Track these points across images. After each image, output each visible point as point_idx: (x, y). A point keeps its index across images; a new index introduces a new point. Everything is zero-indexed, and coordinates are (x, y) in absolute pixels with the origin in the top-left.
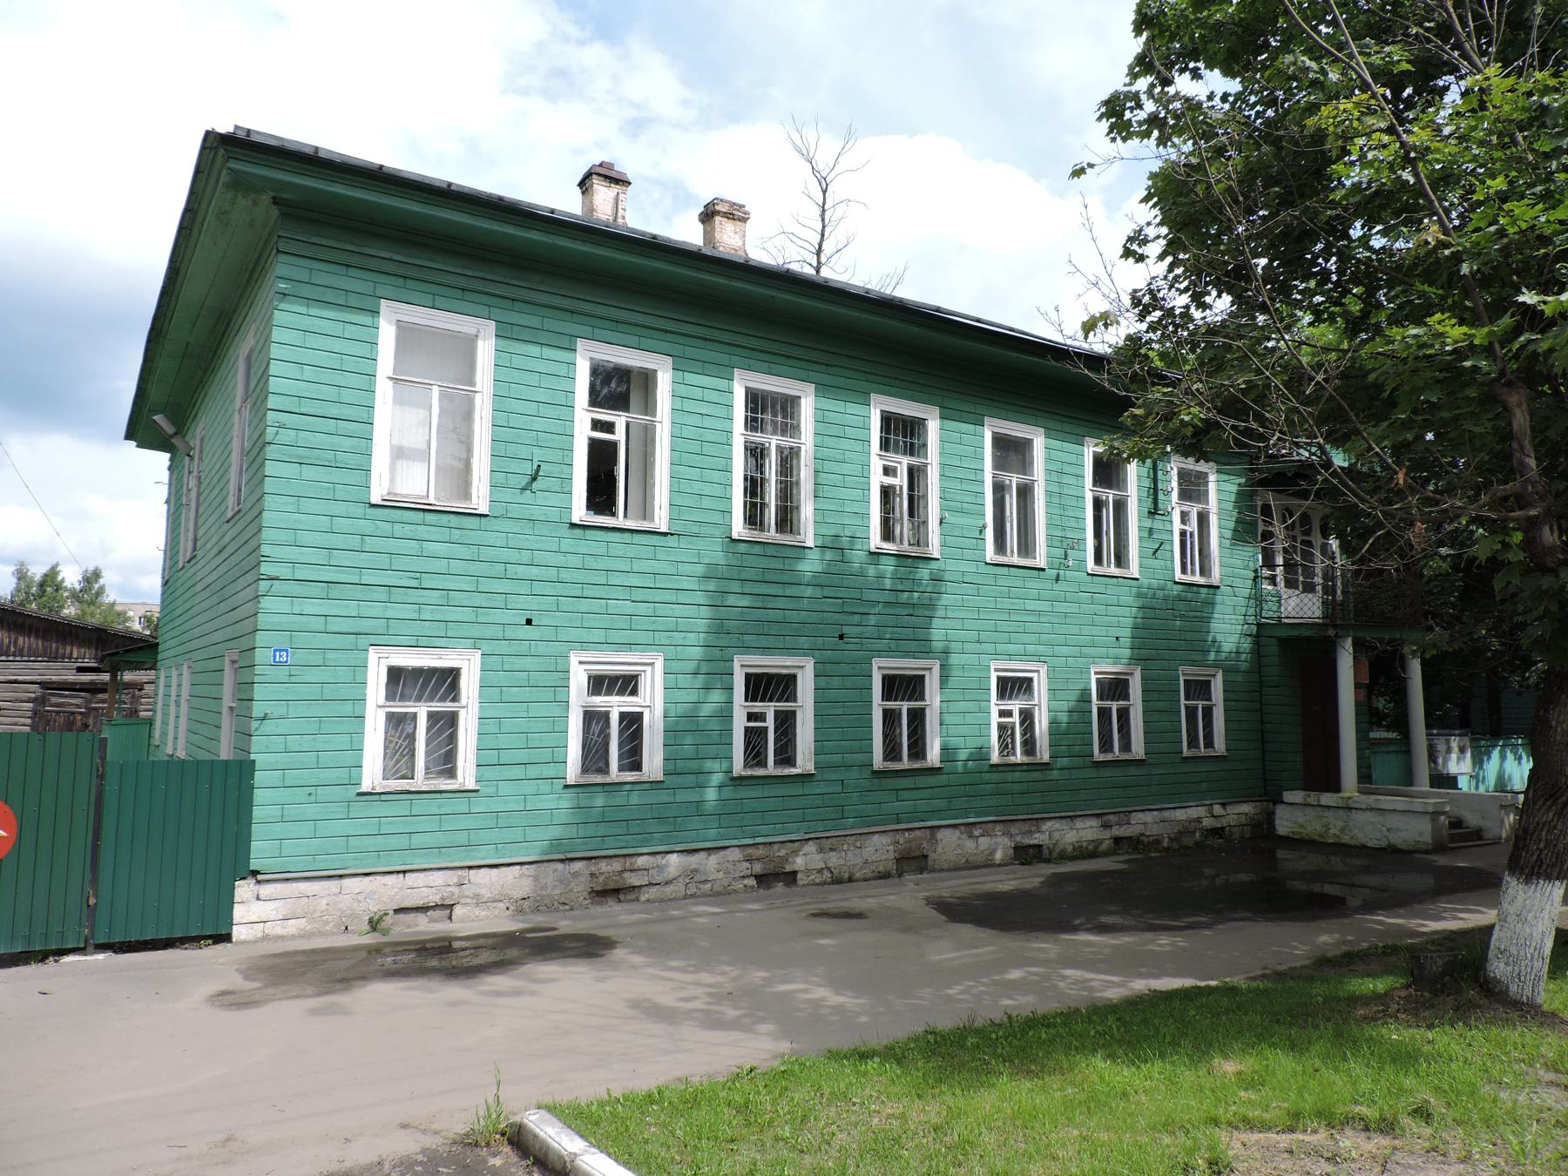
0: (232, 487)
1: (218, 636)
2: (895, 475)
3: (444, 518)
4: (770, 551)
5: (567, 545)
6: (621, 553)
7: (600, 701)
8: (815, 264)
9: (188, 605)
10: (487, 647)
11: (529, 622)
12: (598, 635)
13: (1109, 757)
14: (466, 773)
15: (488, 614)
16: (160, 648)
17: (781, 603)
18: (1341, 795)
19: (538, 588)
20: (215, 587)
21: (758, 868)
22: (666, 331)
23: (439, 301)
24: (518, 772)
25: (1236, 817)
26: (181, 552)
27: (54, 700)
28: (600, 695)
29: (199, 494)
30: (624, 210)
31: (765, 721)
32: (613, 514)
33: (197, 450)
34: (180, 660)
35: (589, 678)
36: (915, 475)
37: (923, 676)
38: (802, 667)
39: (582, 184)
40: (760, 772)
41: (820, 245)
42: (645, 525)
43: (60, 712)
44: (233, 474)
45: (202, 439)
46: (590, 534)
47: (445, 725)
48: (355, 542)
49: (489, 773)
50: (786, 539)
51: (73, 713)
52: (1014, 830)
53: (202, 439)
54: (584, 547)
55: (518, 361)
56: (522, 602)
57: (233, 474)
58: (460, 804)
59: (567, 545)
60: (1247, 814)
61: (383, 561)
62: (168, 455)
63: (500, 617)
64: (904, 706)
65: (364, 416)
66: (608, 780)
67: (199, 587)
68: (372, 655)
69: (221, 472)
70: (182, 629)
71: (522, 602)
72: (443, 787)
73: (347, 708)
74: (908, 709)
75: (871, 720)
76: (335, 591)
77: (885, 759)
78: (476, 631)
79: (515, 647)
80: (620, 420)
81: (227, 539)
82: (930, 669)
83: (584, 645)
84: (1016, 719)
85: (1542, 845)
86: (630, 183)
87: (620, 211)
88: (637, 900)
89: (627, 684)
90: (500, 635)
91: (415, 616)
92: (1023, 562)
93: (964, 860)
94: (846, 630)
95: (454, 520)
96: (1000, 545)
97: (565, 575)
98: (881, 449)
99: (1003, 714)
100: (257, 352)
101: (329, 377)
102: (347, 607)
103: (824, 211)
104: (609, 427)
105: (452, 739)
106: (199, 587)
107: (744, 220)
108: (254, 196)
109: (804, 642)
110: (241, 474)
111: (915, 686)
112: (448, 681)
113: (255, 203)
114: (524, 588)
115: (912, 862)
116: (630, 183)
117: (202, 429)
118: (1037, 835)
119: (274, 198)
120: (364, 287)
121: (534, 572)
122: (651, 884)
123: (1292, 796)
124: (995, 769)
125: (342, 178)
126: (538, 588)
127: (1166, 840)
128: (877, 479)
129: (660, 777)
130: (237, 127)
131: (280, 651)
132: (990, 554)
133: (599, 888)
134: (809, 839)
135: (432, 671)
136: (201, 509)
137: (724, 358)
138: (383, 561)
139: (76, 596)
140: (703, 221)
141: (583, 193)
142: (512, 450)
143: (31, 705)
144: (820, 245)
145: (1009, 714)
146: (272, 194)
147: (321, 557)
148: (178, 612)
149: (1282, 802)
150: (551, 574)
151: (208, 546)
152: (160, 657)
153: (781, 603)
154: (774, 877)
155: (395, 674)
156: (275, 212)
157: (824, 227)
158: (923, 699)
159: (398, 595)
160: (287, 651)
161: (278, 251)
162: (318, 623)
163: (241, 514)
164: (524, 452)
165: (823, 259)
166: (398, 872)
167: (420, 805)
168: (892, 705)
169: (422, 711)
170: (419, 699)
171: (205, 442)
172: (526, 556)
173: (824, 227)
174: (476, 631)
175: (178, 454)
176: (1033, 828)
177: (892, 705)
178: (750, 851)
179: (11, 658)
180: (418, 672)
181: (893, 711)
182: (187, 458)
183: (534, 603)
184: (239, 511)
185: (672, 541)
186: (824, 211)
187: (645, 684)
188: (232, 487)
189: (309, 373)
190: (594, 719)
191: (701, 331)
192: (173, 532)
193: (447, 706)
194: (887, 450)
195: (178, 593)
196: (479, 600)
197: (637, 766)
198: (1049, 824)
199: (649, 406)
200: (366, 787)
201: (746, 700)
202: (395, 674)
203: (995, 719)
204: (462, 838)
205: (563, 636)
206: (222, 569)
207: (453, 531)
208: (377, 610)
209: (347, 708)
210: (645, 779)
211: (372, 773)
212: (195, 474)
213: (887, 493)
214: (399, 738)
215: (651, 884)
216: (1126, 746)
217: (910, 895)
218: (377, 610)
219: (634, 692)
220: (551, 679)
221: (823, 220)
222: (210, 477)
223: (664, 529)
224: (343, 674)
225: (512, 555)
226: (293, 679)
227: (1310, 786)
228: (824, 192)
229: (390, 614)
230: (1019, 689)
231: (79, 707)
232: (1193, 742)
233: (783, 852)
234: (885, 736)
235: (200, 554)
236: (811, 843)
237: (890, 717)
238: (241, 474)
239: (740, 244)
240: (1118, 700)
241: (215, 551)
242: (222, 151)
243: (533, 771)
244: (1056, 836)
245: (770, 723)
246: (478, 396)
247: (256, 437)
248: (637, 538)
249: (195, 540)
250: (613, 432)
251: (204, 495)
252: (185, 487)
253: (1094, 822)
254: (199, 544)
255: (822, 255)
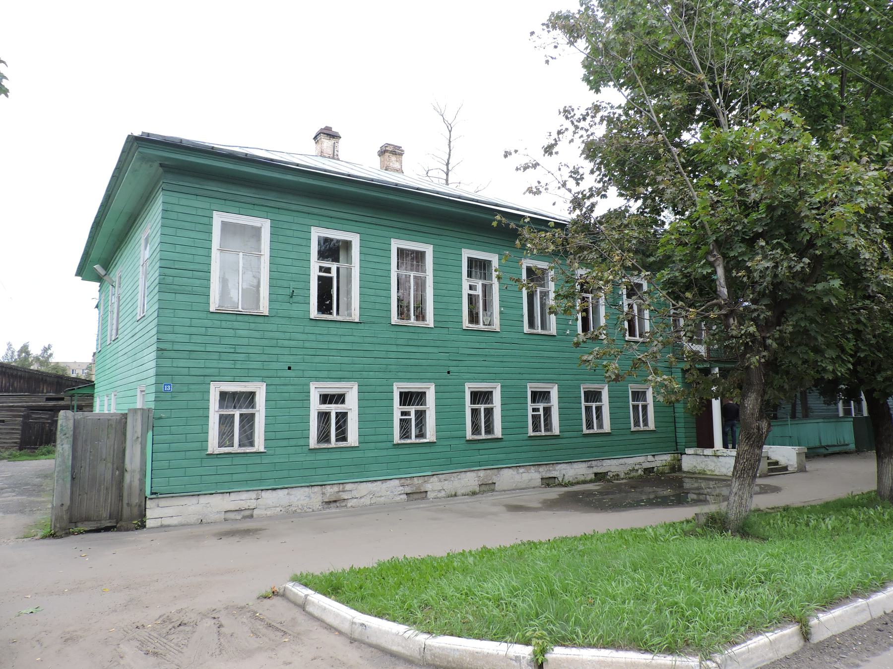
0: (139, 303)
1: (133, 379)
2: (476, 290)
3: (246, 318)
4: (412, 330)
5: (307, 329)
6: (335, 333)
7: (325, 407)
8: (446, 171)
9: (114, 363)
10: (269, 381)
11: (289, 368)
12: (324, 374)
13: (591, 431)
14: (259, 444)
15: (269, 365)
16: (96, 386)
17: (418, 356)
18: (714, 449)
19: (294, 351)
20: (129, 354)
21: (408, 490)
22: (356, 221)
23: (242, 211)
24: (285, 443)
25: (660, 462)
26: (109, 335)
27: (34, 416)
28: (326, 404)
29: (119, 306)
30: (338, 151)
31: (410, 415)
32: (331, 314)
33: (117, 282)
34: (109, 392)
35: (320, 395)
36: (486, 289)
37: (492, 392)
38: (429, 388)
39: (315, 138)
40: (408, 441)
41: (448, 161)
42: (348, 319)
43: (37, 422)
44: (140, 296)
45: (120, 277)
46: (320, 324)
47: (248, 421)
48: (203, 330)
49: (271, 443)
50: (420, 324)
51: (44, 423)
52: (541, 469)
53: (120, 277)
54: (317, 330)
55: (281, 239)
56: (286, 359)
57: (140, 296)
58: (257, 460)
59: (308, 329)
60: (666, 460)
61: (216, 340)
62: (99, 284)
63: (274, 366)
64: (482, 407)
65: (206, 269)
66: (330, 446)
67: (120, 354)
68: (213, 386)
69: (132, 295)
70: (111, 375)
71: (286, 359)
72: (248, 451)
73: (201, 412)
74: (485, 409)
75: (465, 414)
76: (194, 355)
77: (473, 434)
78: (264, 373)
79: (283, 381)
80: (334, 266)
81: (137, 329)
82: (496, 388)
83: (317, 379)
84: (541, 412)
85: (745, 461)
86: (340, 137)
87: (336, 152)
88: (346, 506)
89: (339, 398)
90: (275, 375)
91: (233, 366)
92: (543, 332)
93: (515, 485)
94: (451, 369)
95: (252, 319)
96: (531, 324)
97: (307, 345)
98: (468, 277)
99: (534, 410)
100: (152, 237)
101: (189, 250)
102: (199, 363)
103: (450, 142)
104: (328, 270)
105: (252, 427)
106: (120, 354)
107: (401, 155)
108: (150, 163)
109: (429, 375)
110: (144, 297)
111: (488, 396)
112: (250, 398)
113: (151, 166)
114: (286, 351)
115: (487, 487)
116: (340, 137)
117: (116, 273)
118: (553, 472)
119: (160, 164)
120: (207, 206)
121: (292, 343)
122: (353, 498)
123: (689, 451)
124: (530, 439)
125: (194, 154)
126: (294, 351)
127: (623, 474)
128: (466, 291)
129: (357, 445)
130: (143, 133)
131: (167, 385)
132: (526, 329)
133: (327, 500)
134: (433, 475)
135: (242, 394)
136: (121, 314)
137: (386, 233)
138: (216, 340)
139: (37, 359)
140: (379, 155)
141: (316, 143)
142: (280, 283)
143: (21, 419)
144: (448, 161)
145: (538, 410)
146: (159, 162)
147: (186, 339)
148: (107, 367)
149: (685, 454)
150: (300, 344)
151: (126, 333)
152: (96, 391)
153: (418, 356)
154: (417, 495)
155: (223, 395)
156: (161, 170)
157: (450, 151)
158: (492, 403)
159: (224, 356)
160: (170, 385)
161: (163, 189)
162: (186, 371)
163: (144, 318)
164: (285, 284)
165: (450, 167)
166: (227, 493)
167: (237, 460)
168: (476, 406)
169: (237, 414)
170: (235, 408)
171: (122, 279)
172: (287, 336)
173: (450, 151)
174: (264, 373)
175: (105, 284)
176: (551, 468)
177: (476, 406)
178: (403, 481)
179: (10, 394)
180: (234, 394)
181: (476, 410)
182: (111, 286)
183: (292, 358)
184: (144, 316)
185: (361, 326)
186: (450, 142)
187: (348, 398)
188: (139, 303)
189: (179, 248)
190: (324, 417)
191: (374, 220)
192: (102, 324)
193: (250, 411)
194: (471, 277)
195: (107, 357)
196: (265, 358)
197: (344, 439)
198: (560, 466)
199: (349, 260)
200: (210, 451)
201: (400, 405)
202: (223, 395)
203: (530, 413)
204: (257, 476)
205: (306, 374)
206: (134, 345)
207: (251, 324)
208: (214, 364)
209: (201, 412)
210: (348, 445)
211: (213, 445)
212: (116, 295)
213: (472, 299)
214: (226, 427)
215: (353, 498)
216: (600, 426)
217: (485, 502)
218: (214, 364)
219: (343, 402)
220: (301, 396)
221: (450, 147)
222: (126, 297)
223: (357, 320)
224: (198, 396)
225: (281, 335)
226: (173, 399)
227: (699, 446)
228: (450, 132)
229: (221, 366)
230: (543, 397)
231: (47, 419)
232: (637, 423)
233: (420, 482)
234: (473, 423)
235: (120, 337)
236: (435, 477)
237: (475, 412)
238: (144, 297)
239: (399, 167)
240: (596, 402)
241: (130, 335)
242: (136, 144)
243: (293, 442)
244: (563, 472)
245: (413, 416)
246: (262, 258)
247: (153, 280)
248: (343, 325)
249: (117, 330)
250: (330, 273)
251: (122, 306)
252: (110, 302)
253: (584, 465)
254: (119, 332)
255: (449, 165)
